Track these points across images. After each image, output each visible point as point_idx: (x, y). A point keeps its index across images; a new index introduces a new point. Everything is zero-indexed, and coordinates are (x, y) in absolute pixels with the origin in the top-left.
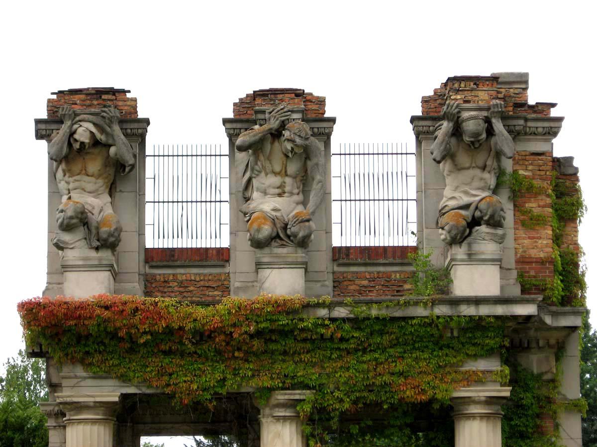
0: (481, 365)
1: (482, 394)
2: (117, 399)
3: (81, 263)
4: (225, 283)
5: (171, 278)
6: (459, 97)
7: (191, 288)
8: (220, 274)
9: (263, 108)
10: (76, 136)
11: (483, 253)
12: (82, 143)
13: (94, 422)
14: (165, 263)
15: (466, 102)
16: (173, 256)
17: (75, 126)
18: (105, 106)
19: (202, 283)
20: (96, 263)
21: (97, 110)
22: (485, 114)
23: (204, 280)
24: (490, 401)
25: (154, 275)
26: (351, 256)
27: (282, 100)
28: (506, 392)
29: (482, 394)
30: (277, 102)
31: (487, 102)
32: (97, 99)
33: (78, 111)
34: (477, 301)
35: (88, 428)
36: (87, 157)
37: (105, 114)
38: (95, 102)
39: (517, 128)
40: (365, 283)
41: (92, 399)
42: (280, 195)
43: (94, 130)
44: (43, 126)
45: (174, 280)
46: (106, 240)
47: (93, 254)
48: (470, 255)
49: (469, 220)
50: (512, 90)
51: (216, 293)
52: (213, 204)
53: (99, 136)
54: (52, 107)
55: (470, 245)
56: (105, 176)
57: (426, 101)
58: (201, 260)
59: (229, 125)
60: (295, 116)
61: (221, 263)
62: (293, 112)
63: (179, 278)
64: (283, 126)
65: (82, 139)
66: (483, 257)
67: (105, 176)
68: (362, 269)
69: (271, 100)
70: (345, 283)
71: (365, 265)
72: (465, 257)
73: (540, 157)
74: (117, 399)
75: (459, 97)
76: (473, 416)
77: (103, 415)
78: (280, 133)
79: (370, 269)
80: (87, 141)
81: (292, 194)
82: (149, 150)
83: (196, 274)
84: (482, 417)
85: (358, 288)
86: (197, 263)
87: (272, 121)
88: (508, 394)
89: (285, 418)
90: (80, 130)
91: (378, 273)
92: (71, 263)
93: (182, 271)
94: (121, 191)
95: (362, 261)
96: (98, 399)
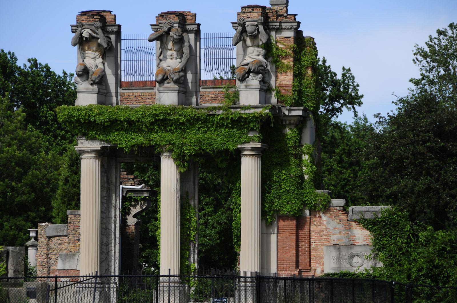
0: (251, 135)
1: (249, 146)
2: (99, 149)
3: (85, 90)
4: (154, 96)
5: (131, 94)
6: (245, 15)
7: (140, 99)
8: (152, 92)
9: (161, 22)
10: (83, 35)
11: (252, 85)
12: (86, 38)
13: (91, 158)
14: (129, 88)
15: (248, 17)
16: (132, 85)
17: (83, 30)
18: (95, 21)
19: (144, 97)
20: (91, 90)
21: (92, 23)
22: (256, 23)
23: (145, 95)
24: (253, 149)
25: (124, 93)
26: (207, 84)
27: (170, 18)
28: (259, 145)
29: (249, 146)
30: (168, 19)
31: (257, 17)
32: (92, 18)
33: (84, 24)
34: (251, 107)
35: (88, 160)
36: (90, 43)
37: (95, 25)
38: (91, 20)
39: (277, 27)
40: (213, 96)
41: (89, 149)
42: (171, 59)
43: (91, 32)
44: (74, 28)
45: (133, 95)
46: (94, 81)
47: (90, 86)
48: (246, 86)
49: (247, 71)
50: (279, 8)
51: (150, 101)
52: (208, 37)
53: (94, 34)
54: (16, 58)
55: (247, 82)
56: (99, 51)
57: (239, 15)
58: (144, 86)
59: (153, 27)
60: (175, 25)
61: (152, 88)
62: (174, 23)
63: (135, 94)
64: (170, 29)
65: (86, 36)
66: (252, 87)
67: (99, 51)
68: (212, 90)
69: (165, 18)
70: (205, 96)
71: (213, 88)
72: (244, 87)
73: (288, 39)
74: (99, 149)
75: (245, 15)
76: (246, 156)
77: (95, 155)
78: (177, 30)
79: (215, 90)
80: (88, 37)
81: (177, 58)
82: (123, 37)
83: (141, 93)
84: (250, 155)
85: (210, 98)
86: (142, 88)
87: (165, 28)
88: (260, 146)
89: (169, 157)
90: (84, 32)
91: (219, 91)
92: (81, 91)
93: (134, 91)
94: (108, 57)
95: (212, 87)
96: (92, 149)
